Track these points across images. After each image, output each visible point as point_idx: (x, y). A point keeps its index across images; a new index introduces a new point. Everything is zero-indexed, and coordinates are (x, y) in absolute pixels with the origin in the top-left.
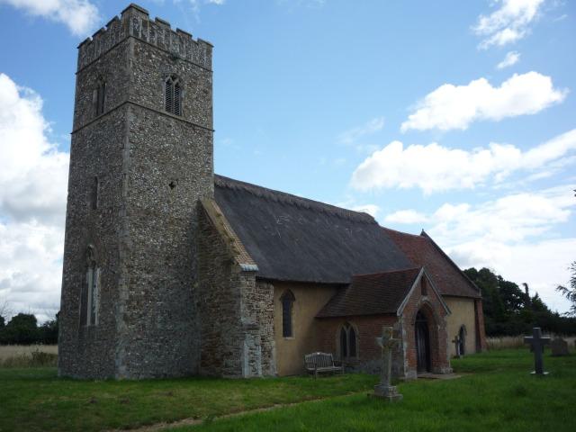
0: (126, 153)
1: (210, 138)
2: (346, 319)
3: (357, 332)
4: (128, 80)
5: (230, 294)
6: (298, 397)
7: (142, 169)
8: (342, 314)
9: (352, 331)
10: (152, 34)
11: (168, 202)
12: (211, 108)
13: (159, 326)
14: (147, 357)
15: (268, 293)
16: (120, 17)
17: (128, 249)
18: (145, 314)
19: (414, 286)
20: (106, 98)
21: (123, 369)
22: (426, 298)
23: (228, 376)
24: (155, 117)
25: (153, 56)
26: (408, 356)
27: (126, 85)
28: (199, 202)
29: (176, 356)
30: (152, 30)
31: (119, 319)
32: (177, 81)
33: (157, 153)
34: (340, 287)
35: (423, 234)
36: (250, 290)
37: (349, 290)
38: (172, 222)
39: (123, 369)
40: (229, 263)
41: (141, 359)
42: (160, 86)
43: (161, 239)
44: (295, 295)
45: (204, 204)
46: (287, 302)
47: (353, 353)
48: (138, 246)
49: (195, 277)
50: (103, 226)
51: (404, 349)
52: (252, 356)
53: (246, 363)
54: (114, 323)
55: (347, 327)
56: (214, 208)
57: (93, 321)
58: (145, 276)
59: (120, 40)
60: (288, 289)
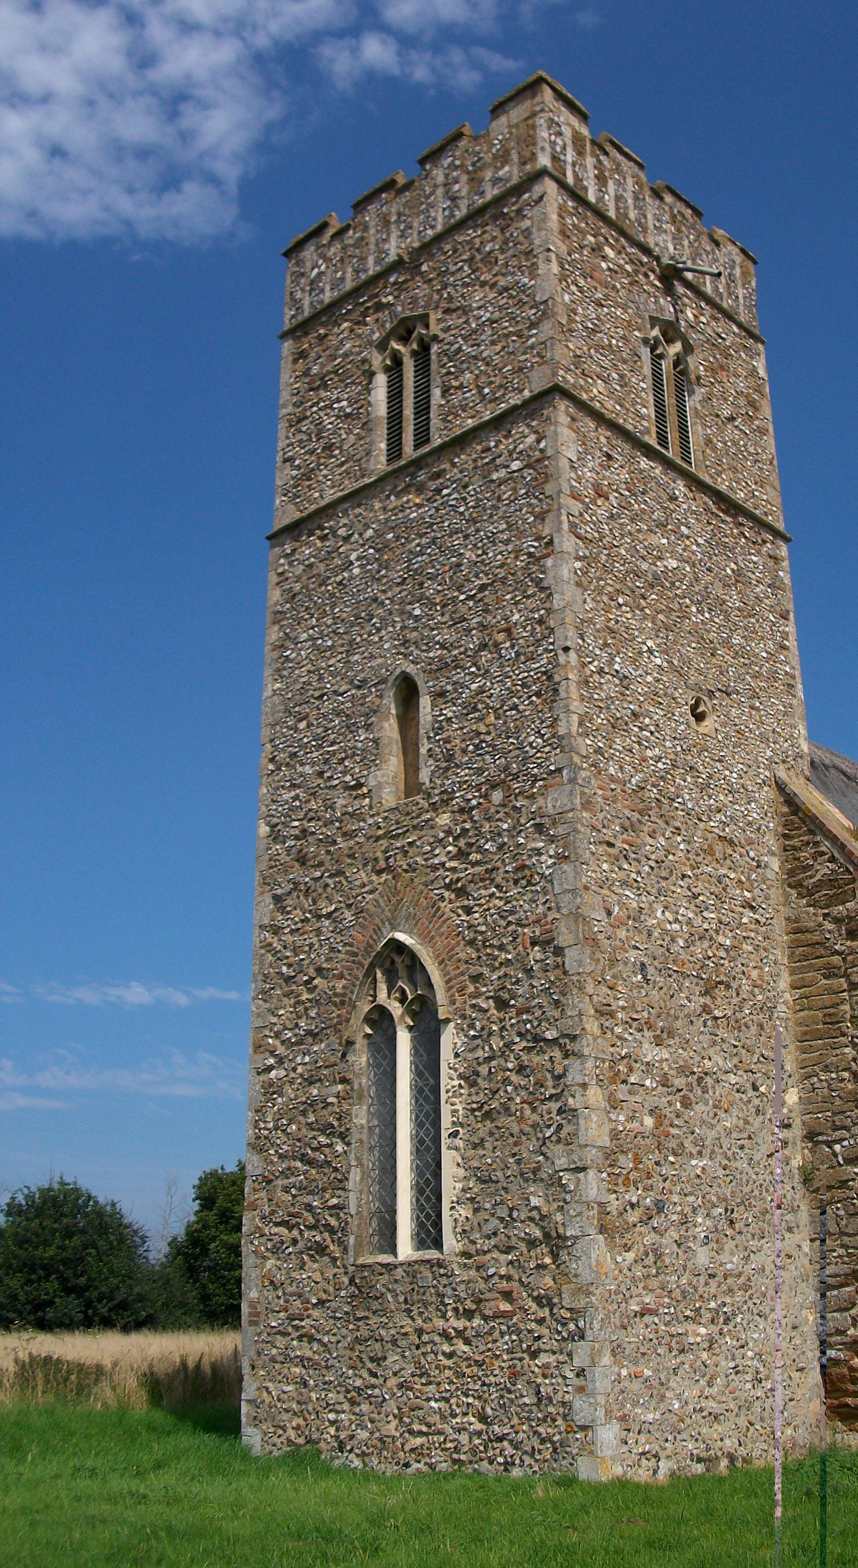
0: (564, 570)
13: (702, 1257)
18: (660, 1207)
20: (436, 393)
25: (610, 253)
26: (836, 1399)
30: (599, 166)
38: (710, 851)
39: (608, 1435)
41: (657, 1392)
48: (622, 934)
50: (461, 855)
55: (834, 1251)
57: (429, 1233)
58: (650, 1053)
59: (491, 193)
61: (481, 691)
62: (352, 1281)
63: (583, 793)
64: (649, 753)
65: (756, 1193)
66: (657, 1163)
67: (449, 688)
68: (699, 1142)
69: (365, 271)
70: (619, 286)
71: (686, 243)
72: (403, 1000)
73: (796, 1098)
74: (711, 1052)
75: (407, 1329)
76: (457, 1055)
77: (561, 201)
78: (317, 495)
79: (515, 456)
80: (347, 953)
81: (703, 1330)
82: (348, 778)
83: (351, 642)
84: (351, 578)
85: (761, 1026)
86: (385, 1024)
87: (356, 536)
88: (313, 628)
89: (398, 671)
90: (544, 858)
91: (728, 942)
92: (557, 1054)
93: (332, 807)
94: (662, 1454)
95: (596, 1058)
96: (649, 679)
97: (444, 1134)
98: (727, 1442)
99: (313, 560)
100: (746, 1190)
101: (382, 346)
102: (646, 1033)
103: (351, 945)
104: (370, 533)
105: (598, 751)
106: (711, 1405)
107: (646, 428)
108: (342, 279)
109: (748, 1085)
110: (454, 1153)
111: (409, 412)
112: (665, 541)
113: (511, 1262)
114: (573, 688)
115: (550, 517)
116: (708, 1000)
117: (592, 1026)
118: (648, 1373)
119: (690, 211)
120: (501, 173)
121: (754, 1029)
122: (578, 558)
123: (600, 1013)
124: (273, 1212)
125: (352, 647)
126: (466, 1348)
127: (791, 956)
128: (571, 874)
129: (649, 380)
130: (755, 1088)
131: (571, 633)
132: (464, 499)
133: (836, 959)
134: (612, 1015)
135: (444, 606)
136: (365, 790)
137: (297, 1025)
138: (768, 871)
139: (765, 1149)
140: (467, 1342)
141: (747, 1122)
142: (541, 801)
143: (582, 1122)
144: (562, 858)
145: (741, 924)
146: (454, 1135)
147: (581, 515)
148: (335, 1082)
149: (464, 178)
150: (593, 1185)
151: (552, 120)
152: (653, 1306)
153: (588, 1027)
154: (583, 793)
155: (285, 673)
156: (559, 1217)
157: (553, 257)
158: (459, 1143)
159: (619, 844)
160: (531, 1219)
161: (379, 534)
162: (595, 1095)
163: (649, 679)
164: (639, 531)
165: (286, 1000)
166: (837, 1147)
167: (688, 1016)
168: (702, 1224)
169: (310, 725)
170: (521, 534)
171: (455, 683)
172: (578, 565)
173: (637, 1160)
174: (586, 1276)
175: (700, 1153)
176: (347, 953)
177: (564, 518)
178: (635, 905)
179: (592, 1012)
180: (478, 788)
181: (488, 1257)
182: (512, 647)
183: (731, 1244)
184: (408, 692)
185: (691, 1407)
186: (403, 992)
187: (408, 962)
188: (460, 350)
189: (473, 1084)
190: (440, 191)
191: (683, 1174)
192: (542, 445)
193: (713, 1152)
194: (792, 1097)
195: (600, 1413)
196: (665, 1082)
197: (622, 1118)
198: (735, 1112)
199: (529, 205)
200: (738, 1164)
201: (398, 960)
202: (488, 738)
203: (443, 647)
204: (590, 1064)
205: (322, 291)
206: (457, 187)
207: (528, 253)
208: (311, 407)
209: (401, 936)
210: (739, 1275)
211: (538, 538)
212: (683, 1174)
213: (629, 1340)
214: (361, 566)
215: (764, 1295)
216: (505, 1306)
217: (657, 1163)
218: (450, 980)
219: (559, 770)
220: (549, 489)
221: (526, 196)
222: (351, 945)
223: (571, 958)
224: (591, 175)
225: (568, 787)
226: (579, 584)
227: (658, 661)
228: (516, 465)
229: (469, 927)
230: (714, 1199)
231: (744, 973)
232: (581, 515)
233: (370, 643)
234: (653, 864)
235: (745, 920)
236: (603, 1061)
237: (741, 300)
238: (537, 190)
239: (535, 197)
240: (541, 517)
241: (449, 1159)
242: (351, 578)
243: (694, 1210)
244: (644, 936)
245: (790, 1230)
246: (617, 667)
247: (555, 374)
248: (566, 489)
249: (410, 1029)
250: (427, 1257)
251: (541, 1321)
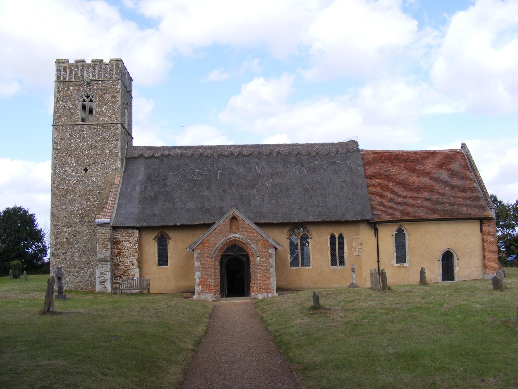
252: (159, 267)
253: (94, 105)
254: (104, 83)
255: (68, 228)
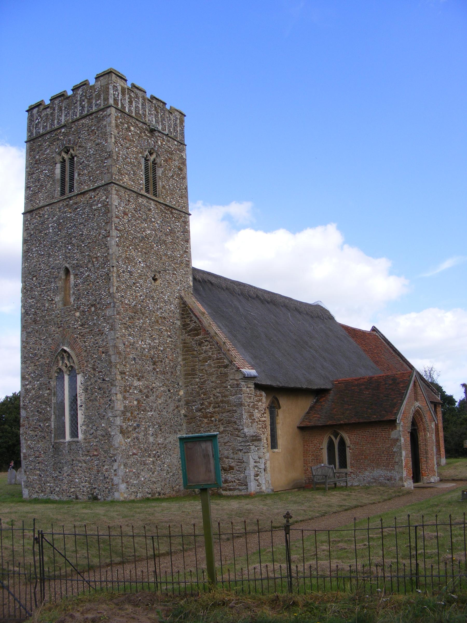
0: (113, 242)
1: (186, 223)
2: (334, 428)
3: (348, 442)
4: (110, 156)
5: (228, 402)
6: (318, 515)
7: (129, 260)
8: (330, 423)
9: (342, 443)
10: (131, 102)
11: (153, 297)
12: (186, 188)
13: (151, 439)
14: (143, 473)
15: (260, 400)
16: (92, 82)
17: (120, 353)
18: (138, 426)
19: (409, 391)
20: (76, 175)
21: (123, 486)
22: (417, 404)
23: (228, 493)
24: (136, 200)
25: (132, 128)
27: (109, 162)
28: (181, 298)
29: (168, 473)
30: (130, 98)
31: (115, 432)
32: (154, 156)
33: (141, 241)
34: (320, 393)
35: (374, 329)
36: (250, 398)
37: (330, 396)
38: (157, 321)
39: (123, 486)
40: (225, 365)
41: (137, 476)
42: (139, 163)
43: (148, 341)
44: (281, 403)
45: (185, 299)
46: (273, 408)
47: (343, 464)
48: (128, 350)
49: (180, 384)
51: (403, 458)
52: (256, 469)
53: (252, 477)
54: (108, 436)
56: (198, 306)
57: (74, 434)
58: (136, 383)
59: (94, 109)
60: (275, 393)
61: (88, 276)
62: (53, 447)
63: (117, 310)
64: (139, 294)
65: (169, 421)
66: (138, 414)
67: (79, 273)
68: (151, 407)
69: (54, 125)
70: (135, 140)
71: (160, 116)
72: (66, 366)
73: (183, 393)
74: (155, 381)
75: (69, 460)
76: (82, 384)
77: (116, 115)
78: (38, 202)
79: (99, 202)
80: (50, 351)
81: (151, 459)
82: (49, 298)
83: (49, 254)
84: (49, 233)
85: (172, 372)
86: (61, 373)
87: (51, 219)
88: (37, 247)
89: (64, 266)
90: (106, 329)
91: (162, 349)
92: (109, 385)
93: (44, 306)
94: (138, 492)
95: (120, 386)
96: (139, 271)
97: (78, 406)
98: (158, 489)
99: (37, 224)
100: (165, 420)
101: (60, 154)
102: (135, 378)
103: (51, 349)
104: (55, 218)
105: (122, 296)
106: (154, 479)
107: (141, 188)
108: (46, 126)
109: (167, 390)
110: (81, 411)
111: (67, 179)
112: (146, 225)
113: (97, 441)
114: (115, 279)
115: (109, 224)
116: (155, 366)
117: (119, 377)
118: (134, 471)
119: (162, 104)
120: (98, 102)
121: (169, 374)
122: (117, 237)
123: (121, 373)
124: (29, 427)
125: (49, 256)
126: (85, 465)
127: (183, 350)
128: (113, 334)
129: (144, 171)
130: (169, 391)
131: (115, 261)
132: (84, 213)
133: (195, 353)
134: (125, 373)
135: (78, 247)
136: (54, 302)
137: (35, 372)
138: (176, 325)
139: (172, 408)
140: (85, 463)
141: (166, 401)
142: (105, 312)
143: (116, 404)
144: (111, 329)
145: (166, 342)
146: (81, 406)
147: (119, 223)
148: (47, 390)
149: (86, 100)
150: (118, 421)
151: (114, 86)
152: (136, 453)
153: (117, 377)
154: (117, 310)
155: (29, 261)
156: (109, 429)
157: (113, 136)
158: (83, 408)
159: (128, 324)
160: (102, 430)
161: (58, 219)
162: (120, 396)
163: (139, 271)
164: (137, 224)
165: (31, 364)
166: (194, 408)
167: (148, 371)
168: (151, 431)
169: (37, 279)
170: (101, 228)
171: (81, 272)
172: (117, 239)
173: (132, 413)
174: (117, 445)
175: (151, 410)
176: (50, 351)
177: (113, 225)
178: (132, 341)
179: (119, 373)
180: (88, 305)
181: (91, 440)
182: (98, 263)
183: (160, 435)
184: (67, 271)
185: (147, 480)
186: (66, 364)
187: (67, 355)
188: (83, 162)
189: (86, 392)
190: (78, 103)
191: (146, 417)
192: (107, 200)
193: (155, 410)
194: (181, 393)
195: (121, 481)
196: (141, 391)
197: (127, 402)
198: (162, 398)
199: (106, 116)
200: (163, 413)
201: (65, 355)
202: (91, 291)
203: (77, 260)
204: (118, 388)
205: (40, 129)
206: (83, 103)
207: (105, 134)
208: (36, 170)
209: (65, 348)
210: (163, 444)
211: (106, 230)
212: (146, 417)
213: (129, 462)
214: (53, 229)
215: (170, 449)
216: (96, 453)
217: (138, 414)
218: (80, 362)
219: (110, 303)
220: (109, 215)
221: (105, 113)
222: (51, 349)
223: (113, 357)
224: (127, 102)
225: (113, 309)
226: (117, 245)
227: (142, 265)
228: (100, 205)
229: (85, 347)
230: (155, 423)
231: (167, 357)
232: (119, 223)
233: (56, 255)
234: (138, 328)
235: (168, 341)
236: (122, 387)
237: (179, 132)
238: (109, 110)
239: (108, 114)
240: (106, 223)
241: (80, 412)
242: (49, 233)
243: (149, 426)
244: (135, 350)
245: (179, 431)
246: (129, 269)
247: (112, 177)
248: (114, 215)
249: (69, 375)
250: (74, 440)
251: (105, 457)
252: (272, 450)
253: (159, 172)
254: (169, 141)
255: (139, 380)
